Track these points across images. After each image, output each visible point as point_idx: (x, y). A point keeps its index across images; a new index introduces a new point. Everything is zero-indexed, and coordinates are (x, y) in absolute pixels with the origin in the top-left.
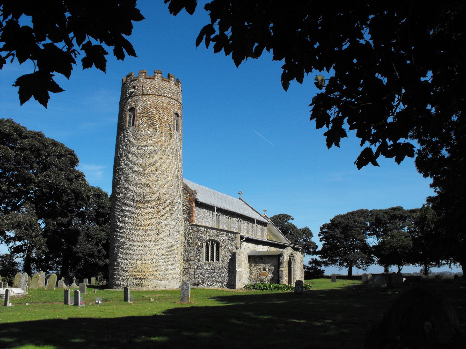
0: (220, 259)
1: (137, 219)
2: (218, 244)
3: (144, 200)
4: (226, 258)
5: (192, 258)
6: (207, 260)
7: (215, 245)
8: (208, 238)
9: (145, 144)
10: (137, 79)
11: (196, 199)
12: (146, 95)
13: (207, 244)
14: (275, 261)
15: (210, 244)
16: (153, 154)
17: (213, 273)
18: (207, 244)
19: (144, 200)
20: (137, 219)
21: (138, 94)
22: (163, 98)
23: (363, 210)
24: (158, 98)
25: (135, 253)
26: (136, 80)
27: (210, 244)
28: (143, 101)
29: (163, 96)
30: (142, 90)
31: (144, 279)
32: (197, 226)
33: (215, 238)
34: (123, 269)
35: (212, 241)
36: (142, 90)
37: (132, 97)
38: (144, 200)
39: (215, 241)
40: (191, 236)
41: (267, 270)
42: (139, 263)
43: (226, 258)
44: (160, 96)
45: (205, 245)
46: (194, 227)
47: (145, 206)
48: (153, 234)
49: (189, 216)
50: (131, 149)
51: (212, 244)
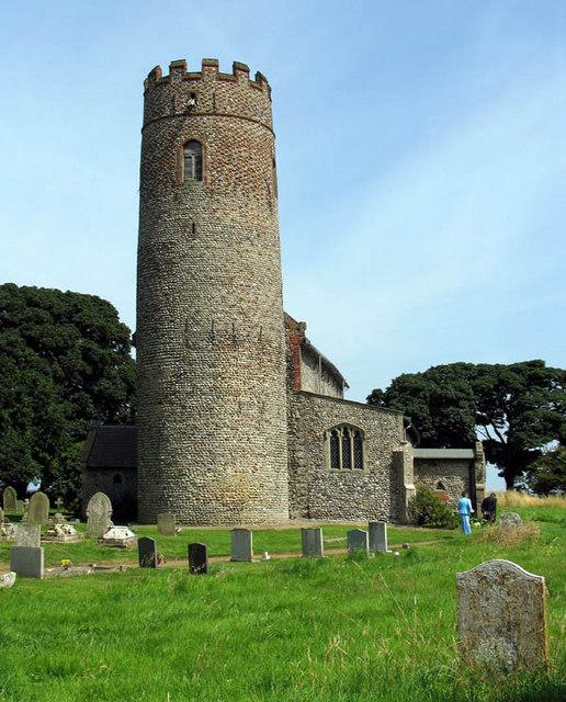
0: (365, 465)
1: (223, 379)
2: (359, 434)
3: (235, 342)
4: (378, 462)
5: (302, 462)
6: (336, 464)
7: (352, 435)
8: (337, 422)
9: (228, 222)
10: (199, 79)
11: (304, 340)
12: (223, 115)
13: (334, 433)
14: (464, 469)
15: (340, 434)
16: (246, 245)
17: (351, 491)
18: (334, 433)
19: (234, 341)
20: (223, 379)
21: (203, 110)
22: (256, 125)
23: (443, 367)
24: (248, 126)
25: (220, 451)
26: (197, 79)
27: (340, 434)
28: (218, 129)
29: (255, 122)
30: (214, 104)
31: (238, 506)
32: (309, 395)
33: (352, 421)
34: (194, 484)
35: (346, 428)
36: (214, 104)
37: (190, 115)
38: (234, 341)
39: (352, 428)
40: (298, 416)
41: (446, 488)
42: (229, 470)
43: (378, 462)
44: (250, 120)
45: (329, 434)
46: (303, 399)
47: (236, 353)
48: (254, 411)
49: (293, 376)
50: (198, 230)
51: (346, 433)
